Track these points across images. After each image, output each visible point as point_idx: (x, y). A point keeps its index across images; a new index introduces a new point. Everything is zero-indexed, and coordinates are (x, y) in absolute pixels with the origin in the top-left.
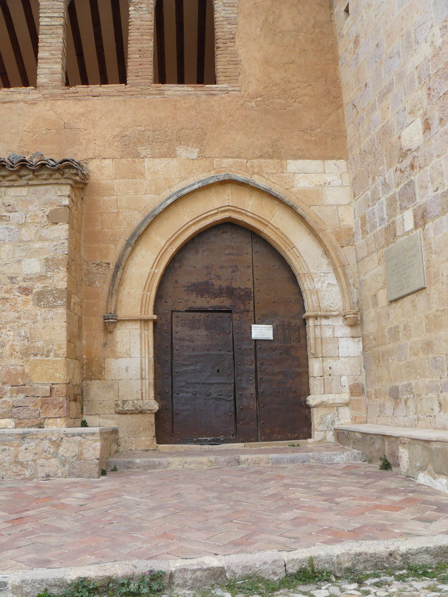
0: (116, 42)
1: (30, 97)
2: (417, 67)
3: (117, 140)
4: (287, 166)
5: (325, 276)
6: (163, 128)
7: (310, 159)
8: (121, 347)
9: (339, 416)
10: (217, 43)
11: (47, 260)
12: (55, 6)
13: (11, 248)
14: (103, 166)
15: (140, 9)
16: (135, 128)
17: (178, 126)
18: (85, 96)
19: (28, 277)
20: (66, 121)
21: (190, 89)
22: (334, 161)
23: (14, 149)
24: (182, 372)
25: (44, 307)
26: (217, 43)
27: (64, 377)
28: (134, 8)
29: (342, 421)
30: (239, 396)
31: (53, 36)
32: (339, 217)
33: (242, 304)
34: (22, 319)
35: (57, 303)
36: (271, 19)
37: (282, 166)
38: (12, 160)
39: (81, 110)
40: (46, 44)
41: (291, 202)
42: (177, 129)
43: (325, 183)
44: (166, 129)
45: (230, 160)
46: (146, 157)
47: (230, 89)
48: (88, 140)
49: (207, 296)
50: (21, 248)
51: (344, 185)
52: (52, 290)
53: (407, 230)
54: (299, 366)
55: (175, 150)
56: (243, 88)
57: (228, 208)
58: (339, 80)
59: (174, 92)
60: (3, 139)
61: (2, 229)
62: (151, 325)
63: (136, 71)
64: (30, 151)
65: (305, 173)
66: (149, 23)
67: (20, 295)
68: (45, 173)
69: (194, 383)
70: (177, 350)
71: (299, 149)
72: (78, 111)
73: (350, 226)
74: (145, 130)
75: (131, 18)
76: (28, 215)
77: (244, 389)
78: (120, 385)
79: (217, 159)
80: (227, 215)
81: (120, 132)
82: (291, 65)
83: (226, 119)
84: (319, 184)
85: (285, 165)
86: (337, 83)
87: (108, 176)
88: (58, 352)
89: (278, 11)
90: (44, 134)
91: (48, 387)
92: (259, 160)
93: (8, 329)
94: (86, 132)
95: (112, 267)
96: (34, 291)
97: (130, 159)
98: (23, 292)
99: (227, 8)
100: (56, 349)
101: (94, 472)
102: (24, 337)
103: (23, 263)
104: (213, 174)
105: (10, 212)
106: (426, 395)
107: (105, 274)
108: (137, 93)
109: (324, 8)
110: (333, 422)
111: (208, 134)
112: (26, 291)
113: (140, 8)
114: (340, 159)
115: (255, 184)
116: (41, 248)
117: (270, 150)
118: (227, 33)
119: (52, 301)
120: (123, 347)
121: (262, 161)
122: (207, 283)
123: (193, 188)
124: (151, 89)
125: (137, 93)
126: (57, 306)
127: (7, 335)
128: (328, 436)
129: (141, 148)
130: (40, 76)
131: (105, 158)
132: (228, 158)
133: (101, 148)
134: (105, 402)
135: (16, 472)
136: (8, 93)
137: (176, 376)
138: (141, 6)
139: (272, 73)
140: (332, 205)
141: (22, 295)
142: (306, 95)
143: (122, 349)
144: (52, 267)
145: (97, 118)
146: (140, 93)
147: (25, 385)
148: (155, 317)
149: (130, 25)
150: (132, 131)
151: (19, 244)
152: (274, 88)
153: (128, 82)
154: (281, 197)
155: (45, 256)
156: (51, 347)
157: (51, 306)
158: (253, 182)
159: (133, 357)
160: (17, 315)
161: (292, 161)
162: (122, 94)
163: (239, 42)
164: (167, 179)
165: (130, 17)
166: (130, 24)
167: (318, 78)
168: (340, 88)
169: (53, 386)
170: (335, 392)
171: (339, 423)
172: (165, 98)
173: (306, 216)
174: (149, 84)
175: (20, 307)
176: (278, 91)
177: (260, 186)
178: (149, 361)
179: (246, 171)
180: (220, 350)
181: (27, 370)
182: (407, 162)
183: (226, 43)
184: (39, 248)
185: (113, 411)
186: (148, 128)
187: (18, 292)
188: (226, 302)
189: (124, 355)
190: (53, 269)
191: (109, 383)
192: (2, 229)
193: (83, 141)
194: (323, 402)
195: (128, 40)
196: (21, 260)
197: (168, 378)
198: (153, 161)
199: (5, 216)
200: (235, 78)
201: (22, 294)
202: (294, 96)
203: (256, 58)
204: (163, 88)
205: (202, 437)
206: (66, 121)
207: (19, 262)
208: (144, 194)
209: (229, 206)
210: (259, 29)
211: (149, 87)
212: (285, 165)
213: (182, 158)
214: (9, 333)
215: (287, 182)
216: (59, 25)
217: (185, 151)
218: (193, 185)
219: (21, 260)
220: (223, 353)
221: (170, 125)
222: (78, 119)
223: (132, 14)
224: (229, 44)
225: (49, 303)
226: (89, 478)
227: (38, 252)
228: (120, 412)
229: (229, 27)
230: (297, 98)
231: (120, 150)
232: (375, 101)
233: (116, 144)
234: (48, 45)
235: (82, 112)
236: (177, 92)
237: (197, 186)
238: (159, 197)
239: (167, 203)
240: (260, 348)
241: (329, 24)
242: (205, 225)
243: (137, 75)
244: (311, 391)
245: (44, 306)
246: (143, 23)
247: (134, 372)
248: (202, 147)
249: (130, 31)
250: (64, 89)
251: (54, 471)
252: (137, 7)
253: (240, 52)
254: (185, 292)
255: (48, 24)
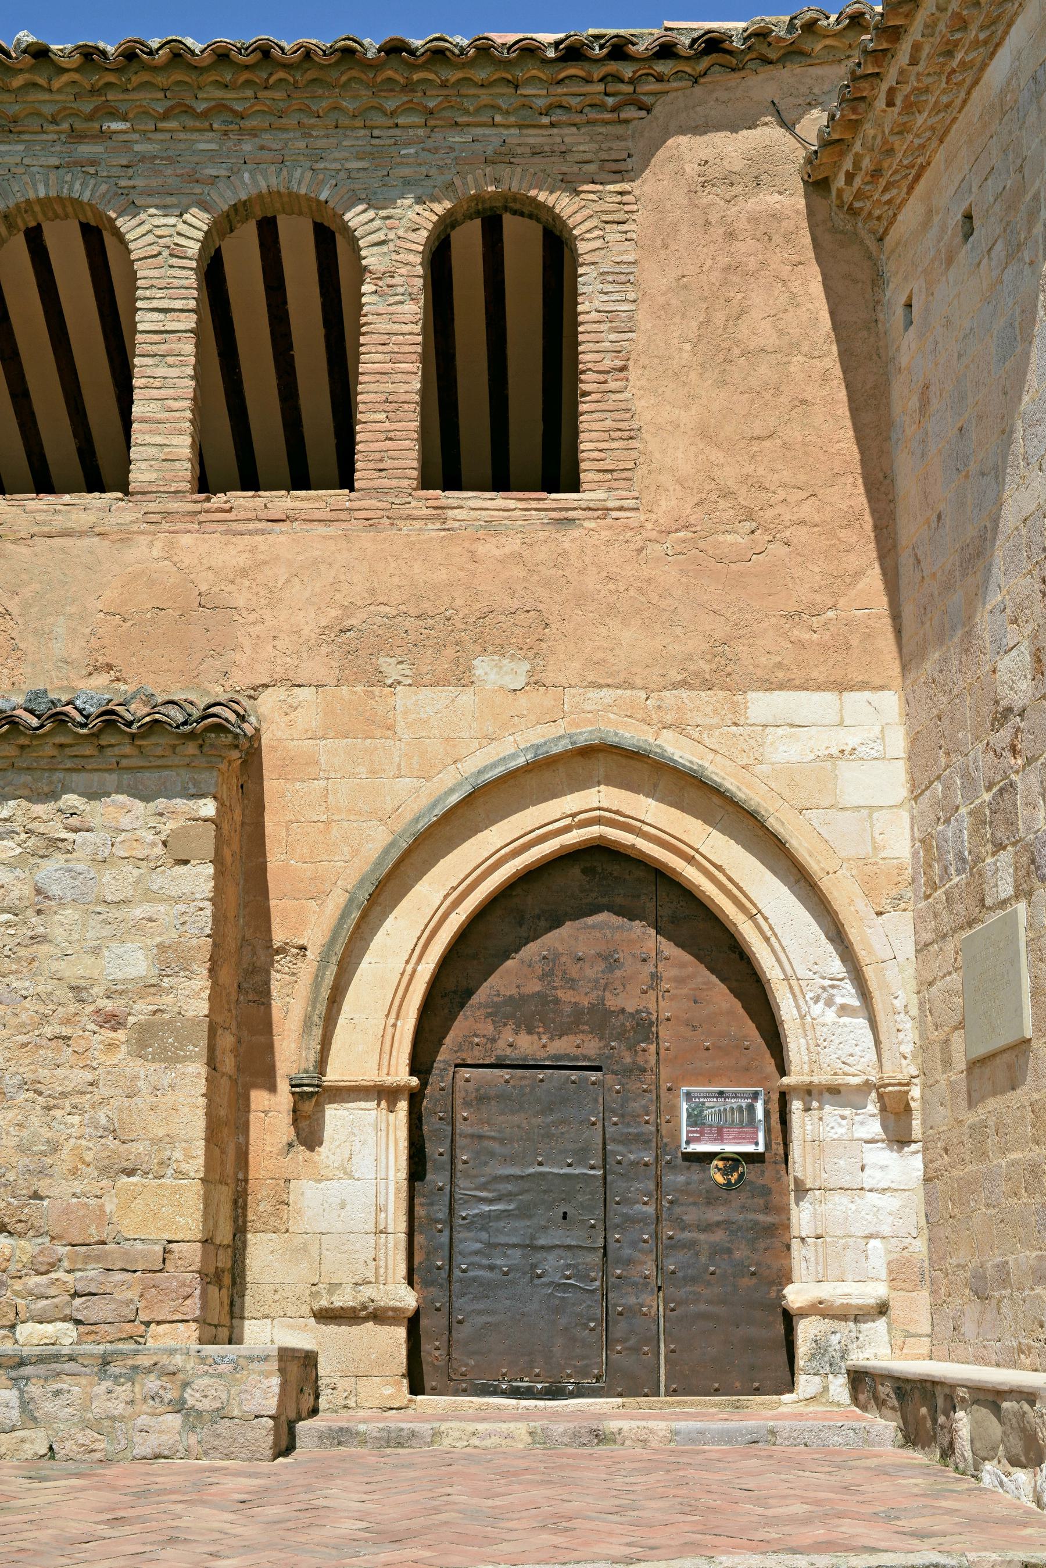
0: (325, 327)
1: (115, 518)
2: (1025, 521)
3: (329, 640)
4: (747, 708)
5: (832, 987)
6: (442, 609)
7: (806, 689)
8: (330, 1154)
9: (861, 1339)
10: (582, 382)
11: (162, 947)
12: (176, 282)
13: (77, 917)
14: (295, 705)
15: (389, 291)
16: (372, 608)
17: (477, 606)
18: (250, 520)
19: (118, 987)
20: (203, 589)
21: (512, 504)
22: (867, 695)
23: (74, 656)
24: (476, 1215)
25: (154, 1060)
26: (582, 382)
27: (197, 1225)
28: (374, 288)
29: (868, 1352)
30: (614, 1279)
31: (170, 360)
32: (873, 838)
33: (629, 1053)
34: (101, 1085)
35: (184, 1051)
36: (719, 318)
37: (735, 709)
38: (81, 706)
39: (242, 560)
40: (151, 380)
41: (752, 803)
42: (477, 613)
43: (842, 751)
44: (447, 613)
45: (605, 691)
46: (399, 683)
47: (611, 504)
48: (258, 637)
49: (541, 1030)
50: (102, 917)
51: (888, 756)
52: (171, 1021)
53: (1003, 896)
54: (767, 1209)
55: (470, 669)
56: (643, 501)
57: (597, 813)
58: (888, 481)
59: (472, 513)
60: (47, 631)
61: (57, 870)
62: (403, 1105)
63: (378, 456)
64: (115, 662)
65: (792, 726)
66: (411, 328)
67: (96, 1028)
68: (157, 743)
69: (503, 1245)
70: (465, 1162)
71: (779, 665)
72: (234, 562)
73: (899, 861)
74: (398, 615)
75: (365, 315)
76: (118, 840)
77: (629, 1262)
78: (324, 1246)
79: (573, 691)
80: (595, 831)
81: (336, 618)
82: (766, 444)
83: (598, 587)
84: (826, 753)
85: (742, 706)
86: (883, 489)
87: (307, 731)
88: (185, 1167)
89: (740, 296)
90: (148, 620)
91: (158, 1249)
92: (676, 692)
93: (69, 1109)
94: (252, 617)
95: (313, 957)
96: (131, 1020)
97: (358, 689)
98: (106, 1022)
99: (610, 288)
100: (181, 1158)
101: (264, 1445)
102: (105, 1129)
103: (107, 954)
104: (560, 729)
105: (76, 830)
106: (1033, 1289)
107: (294, 974)
108: (379, 513)
109: (860, 285)
110: (844, 1354)
111: (553, 626)
112: (112, 1021)
113: (389, 286)
114: (881, 688)
115: (663, 757)
116: (150, 920)
117: (706, 668)
118: (608, 355)
119: (172, 1045)
120: (334, 1154)
121: (684, 695)
122: (542, 998)
123: (513, 764)
124: (414, 503)
125: (379, 513)
126: (184, 1057)
127: (66, 1124)
128: (832, 1387)
129: (388, 659)
130: (138, 464)
131: (299, 686)
132: (601, 686)
133: (288, 659)
134: (285, 1287)
135: (84, 1445)
136: (58, 507)
137: (460, 1225)
138: (391, 281)
139: (717, 465)
140: (858, 808)
141: (103, 1031)
142: (802, 522)
143: (331, 1156)
144: (173, 966)
145: (280, 583)
146: (386, 513)
147: (104, 1243)
148: (414, 1081)
149: (364, 334)
150: (365, 616)
151: (98, 909)
152: (722, 504)
153: (357, 485)
154: (727, 790)
155: (158, 940)
156: (167, 1154)
157: (171, 1057)
158: (658, 750)
159: (359, 1179)
160: (89, 1076)
161: (760, 694)
162: (343, 516)
163: (639, 379)
164: (448, 739)
165: (365, 310)
166: (364, 329)
167: (837, 475)
168: (892, 501)
169: (171, 1245)
170: (850, 1277)
171: (861, 1356)
172: (448, 530)
173: (788, 838)
174: (410, 491)
175: (99, 1057)
176: (731, 512)
177: (675, 761)
178: (397, 1189)
179: (643, 721)
180: (570, 1165)
181: (109, 1208)
182: (1004, 735)
183: (606, 382)
184: (143, 919)
185: (306, 1310)
186: (405, 610)
187: (94, 1021)
188: (591, 1047)
189: (337, 1173)
190: (176, 969)
191: (299, 1239)
192: (57, 870)
193: (247, 642)
194: (821, 1303)
195: (357, 374)
196: (99, 947)
197: (440, 1231)
198: (416, 694)
199: (63, 840)
200: (625, 475)
201: (101, 1027)
202: (772, 526)
203: (679, 426)
204: (444, 502)
205: (522, 1380)
206: (203, 588)
207: (96, 951)
208: (394, 777)
209: (599, 809)
210: (687, 347)
211: (410, 499)
212: (742, 706)
213: (489, 686)
214: (69, 1119)
215: (746, 748)
216: (186, 331)
217: (495, 670)
218: (513, 756)
219: (99, 947)
220: (577, 1172)
221: (459, 602)
222: (232, 583)
223: (369, 304)
224: (613, 385)
225: (165, 1049)
226: (250, 1460)
227: (138, 928)
228: (324, 1313)
229: (613, 337)
230: (779, 531)
231: (335, 664)
232: (954, 565)
233: (325, 649)
234: (157, 384)
235: (242, 564)
236: (479, 512)
237: (521, 761)
238: (429, 784)
239: (447, 802)
240: (668, 1163)
241: (869, 329)
242: (539, 856)
243: (381, 466)
244: (795, 1275)
245: (153, 1057)
246: (396, 327)
247: (361, 1217)
248: (537, 661)
249: (362, 349)
250: (196, 502)
251: (170, 1442)
252: (380, 283)
253: (639, 405)
254: (489, 1020)
255: (157, 328)
